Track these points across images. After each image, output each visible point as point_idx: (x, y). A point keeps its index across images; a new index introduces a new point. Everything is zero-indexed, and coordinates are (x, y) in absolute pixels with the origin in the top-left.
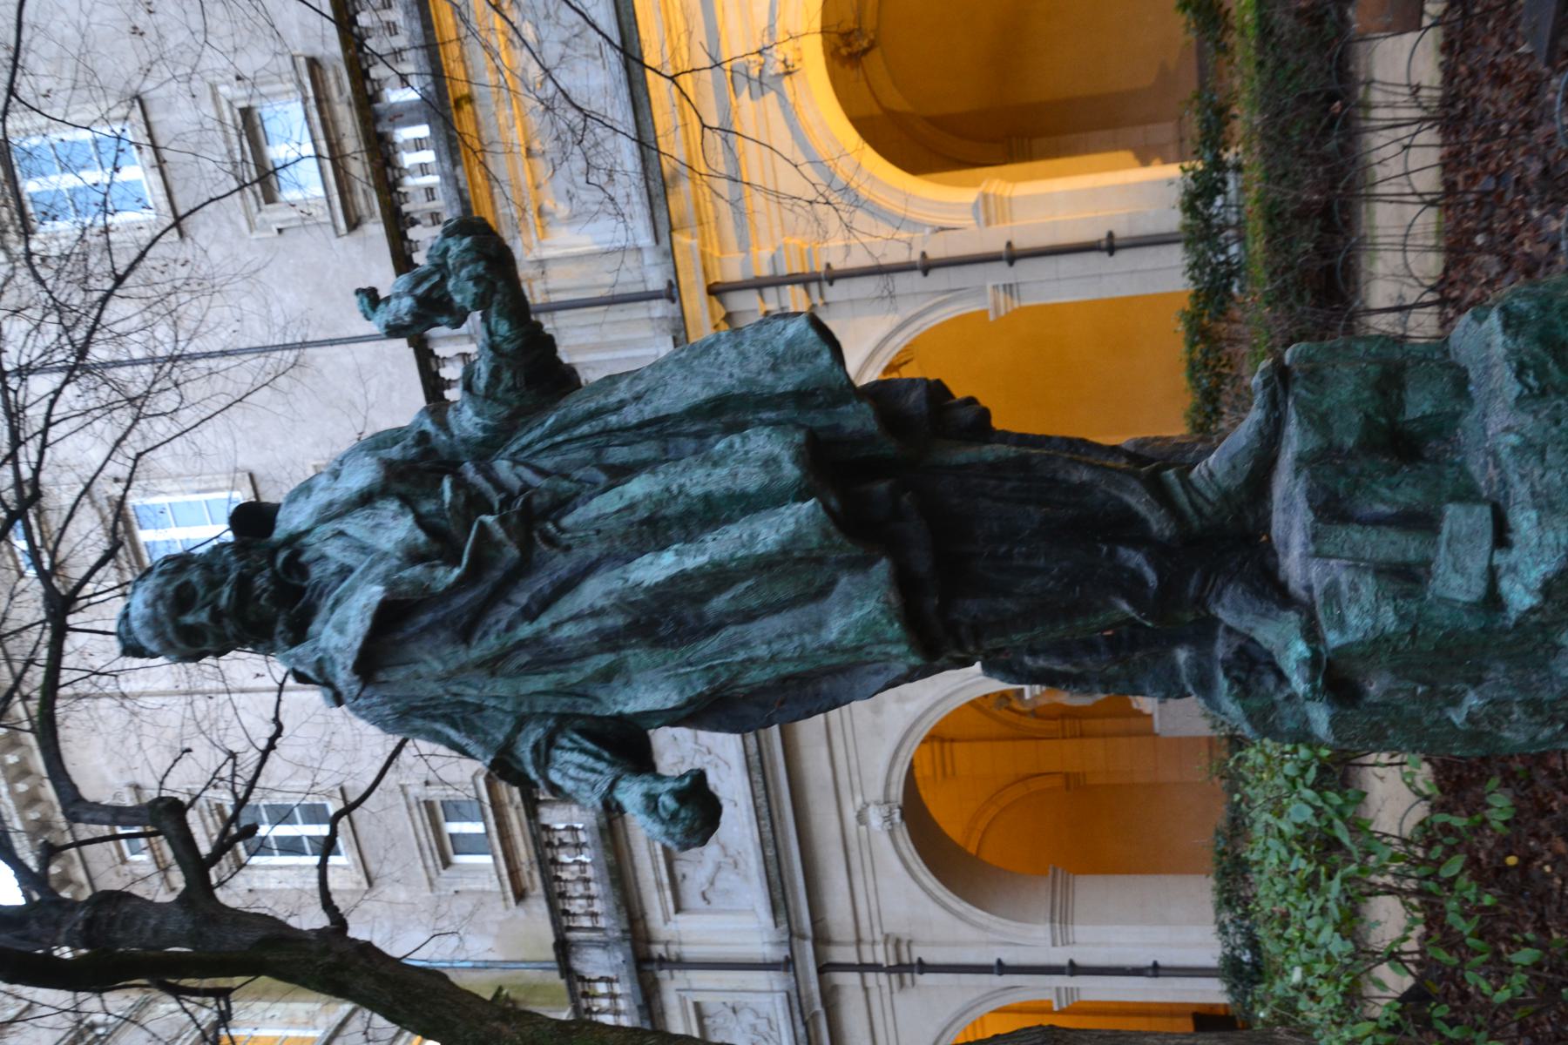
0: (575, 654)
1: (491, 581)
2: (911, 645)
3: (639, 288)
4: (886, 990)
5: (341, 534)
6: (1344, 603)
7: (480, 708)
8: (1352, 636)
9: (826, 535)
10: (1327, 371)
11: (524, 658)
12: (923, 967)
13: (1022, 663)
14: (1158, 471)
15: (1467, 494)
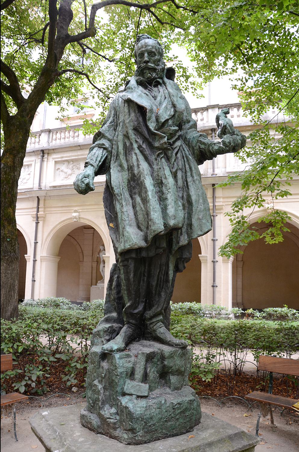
0: (128, 158)
1: (148, 138)
2: (124, 250)
3: (216, 166)
4: (32, 213)
5: (165, 98)
6: (126, 359)
7: (115, 130)
8: (117, 361)
9: (154, 231)
10: (184, 358)
11: (128, 144)
12: (37, 223)
13: (115, 274)
14: (163, 314)
15: (151, 389)
